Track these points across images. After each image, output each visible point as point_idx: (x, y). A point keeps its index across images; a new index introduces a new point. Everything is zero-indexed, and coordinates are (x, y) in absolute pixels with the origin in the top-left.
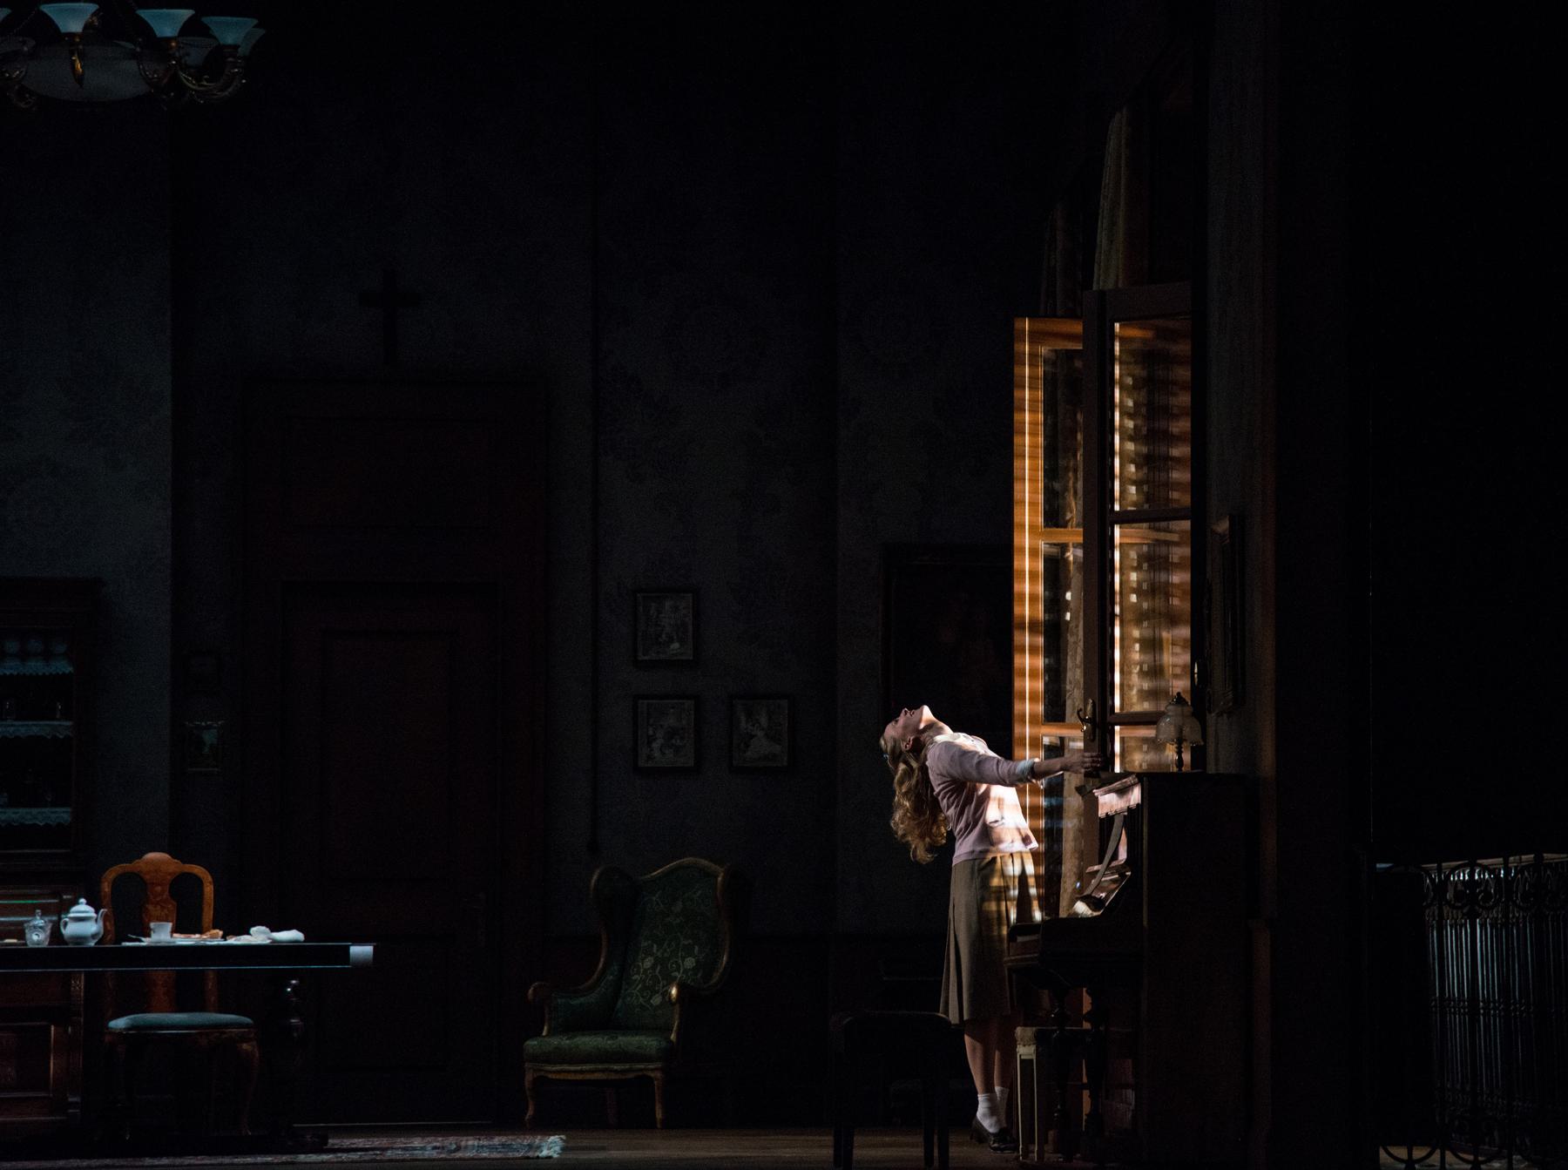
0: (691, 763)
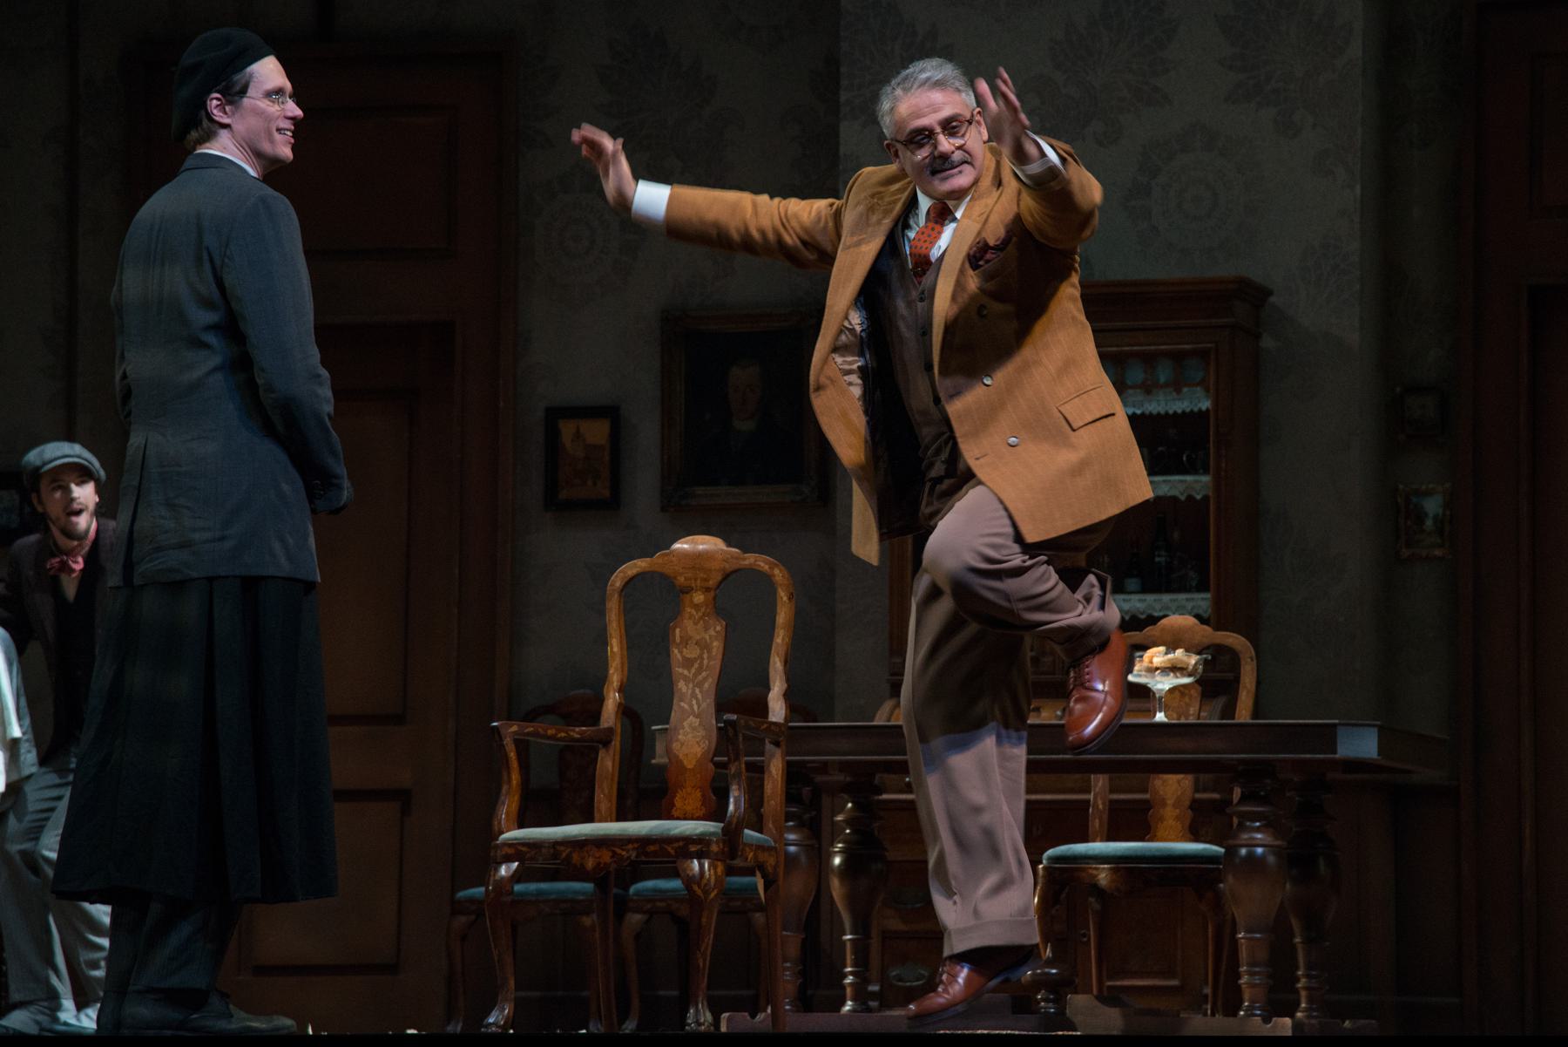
0: (607, 493)
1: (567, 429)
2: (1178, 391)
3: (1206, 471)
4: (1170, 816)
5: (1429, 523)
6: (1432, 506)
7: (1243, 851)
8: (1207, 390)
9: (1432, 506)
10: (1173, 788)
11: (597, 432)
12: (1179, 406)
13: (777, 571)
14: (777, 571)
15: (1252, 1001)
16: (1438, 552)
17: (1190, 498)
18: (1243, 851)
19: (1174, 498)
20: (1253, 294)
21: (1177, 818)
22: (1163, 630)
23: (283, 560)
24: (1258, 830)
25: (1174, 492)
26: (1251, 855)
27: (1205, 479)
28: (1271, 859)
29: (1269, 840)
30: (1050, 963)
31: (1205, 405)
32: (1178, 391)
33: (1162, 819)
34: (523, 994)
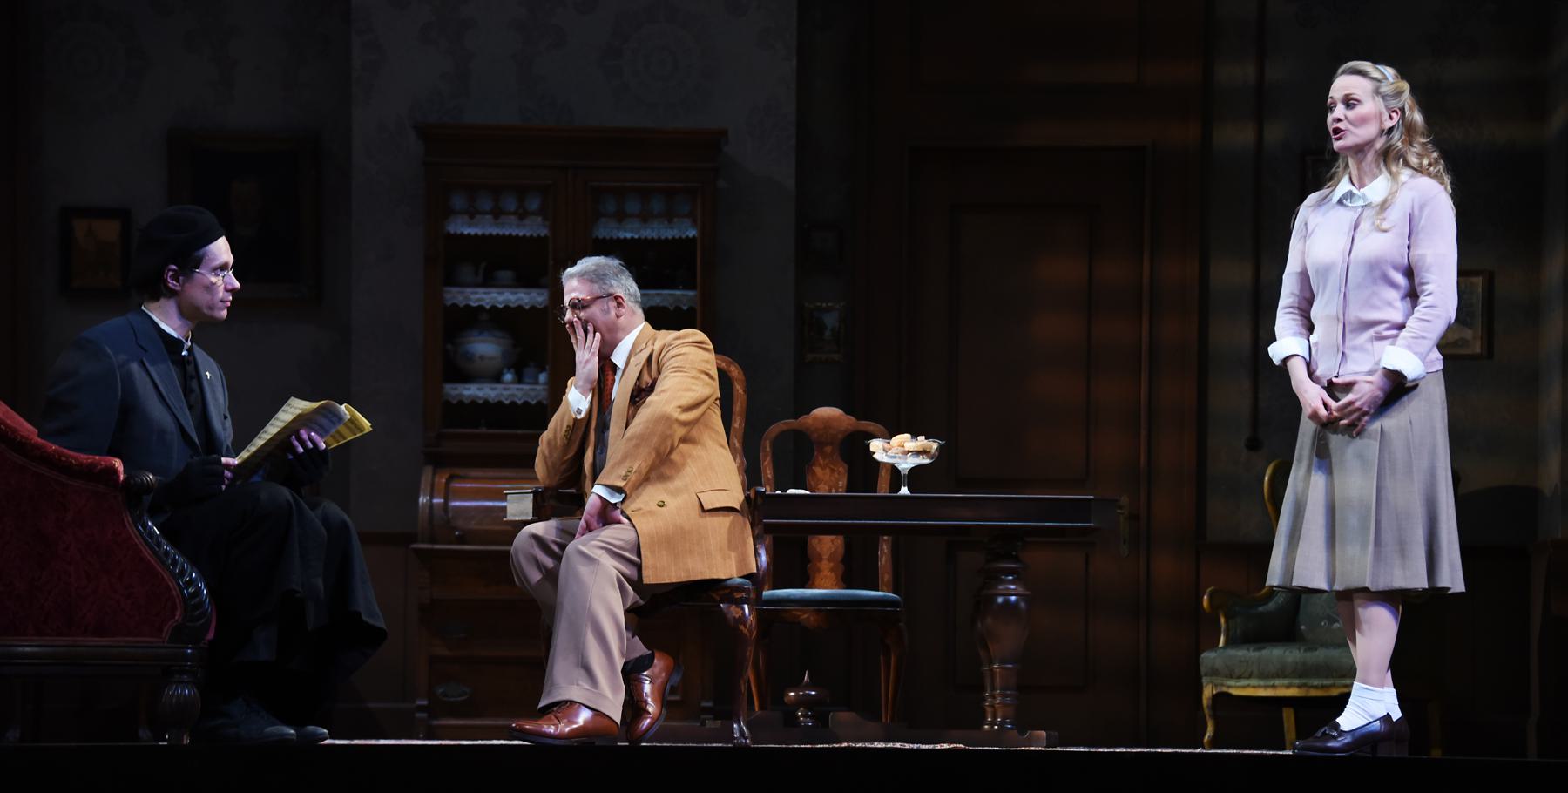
1: (80, 227)
2: (670, 221)
3: (693, 288)
4: (826, 568)
5: (827, 334)
6: (831, 320)
7: (1000, 600)
8: (694, 221)
9: (831, 320)
10: (827, 546)
11: (109, 231)
12: (669, 234)
13: (733, 368)
14: (733, 368)
15: (1004, 718)
16: (836, 357)
17: (678, 309)
18: (1000, 600)
19: (665, 308)
20: (710, 144)
21: (832, 570)
22: (815, 418)
23: (1369, 378)
24: (1011, 582)
25: (665, 304)
26: (1007, 602)
27: (691, 293)
28: (1022, 605)
29: (1021, 590)
30: (810, 686)
31: (692, 233)
32: (670, 221)
33: (819, 571)
34: (886, 718)
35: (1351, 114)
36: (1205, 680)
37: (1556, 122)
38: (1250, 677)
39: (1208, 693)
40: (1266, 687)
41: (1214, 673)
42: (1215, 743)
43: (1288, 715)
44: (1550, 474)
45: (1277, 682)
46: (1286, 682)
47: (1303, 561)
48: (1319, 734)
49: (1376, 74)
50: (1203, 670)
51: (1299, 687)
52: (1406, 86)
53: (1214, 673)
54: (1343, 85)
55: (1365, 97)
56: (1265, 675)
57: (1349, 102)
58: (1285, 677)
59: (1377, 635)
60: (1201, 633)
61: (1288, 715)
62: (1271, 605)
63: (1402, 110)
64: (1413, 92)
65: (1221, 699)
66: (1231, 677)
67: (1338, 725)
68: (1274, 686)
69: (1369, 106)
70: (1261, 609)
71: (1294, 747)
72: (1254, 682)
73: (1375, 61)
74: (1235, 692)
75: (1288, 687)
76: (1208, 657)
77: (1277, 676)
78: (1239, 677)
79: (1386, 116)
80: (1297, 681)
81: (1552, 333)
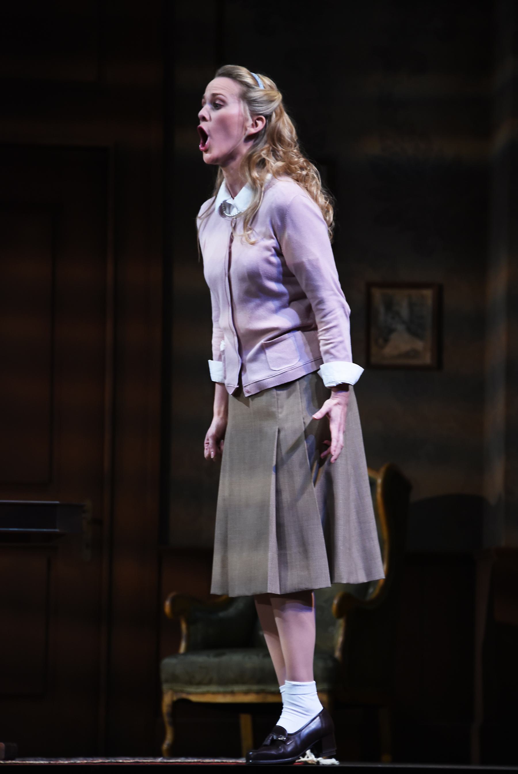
35: (215, 114)
36: (165, 687)
37: (502, 138)
38: (210, 683)
39: (167, 699)
40: (225, 693)
41: (174, 679)
42: (174, 752)
43: (246, 722)
44: (495, 483)
45: (236, 688)
46: (244, 688)
47: (244, 566)
48: (268, 742)
49: (249, 80)
50: (164, 676)
51: (258, 692)
52: (279, 97)
53: (174, 679)
54: (219, 85)
55: (236, 102)
56: (225, 681)
57: (217, 103)
58: (244, 683)
59: (298, 638)
60: (161, 638)
61: (246, 722)
62: (232, 611)
63: (268, 117)
64: (285, 101)
65: (182, 705)
66: (191, 682)
67: (282, 731)
68: (232, 693)
69: (235, 109)
70: (222, 614)
71: (248, 758)
72: (213, 688)
73: (253, 69)
74: (194, 698)
75: (247, 693)
76: (169, 664)
77: (236, 681)
78: (199, 683)
79: (250, 122)
80: (255, 687)
81: (497, 345)
